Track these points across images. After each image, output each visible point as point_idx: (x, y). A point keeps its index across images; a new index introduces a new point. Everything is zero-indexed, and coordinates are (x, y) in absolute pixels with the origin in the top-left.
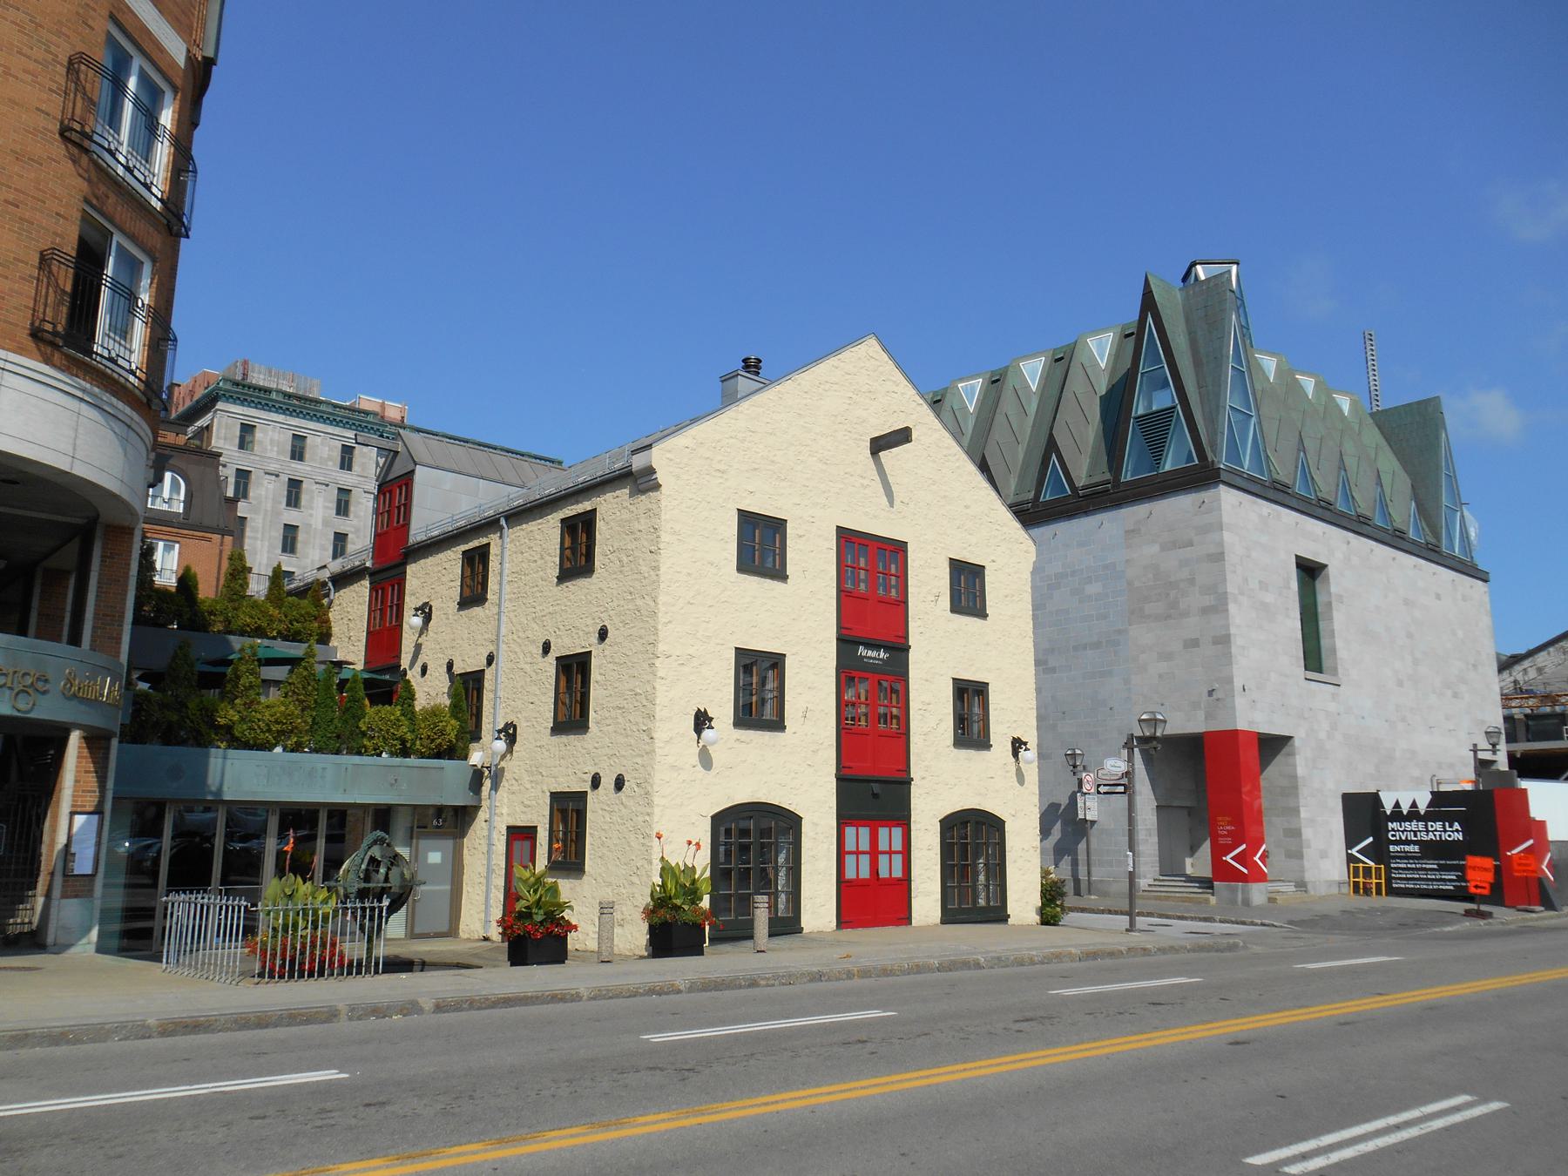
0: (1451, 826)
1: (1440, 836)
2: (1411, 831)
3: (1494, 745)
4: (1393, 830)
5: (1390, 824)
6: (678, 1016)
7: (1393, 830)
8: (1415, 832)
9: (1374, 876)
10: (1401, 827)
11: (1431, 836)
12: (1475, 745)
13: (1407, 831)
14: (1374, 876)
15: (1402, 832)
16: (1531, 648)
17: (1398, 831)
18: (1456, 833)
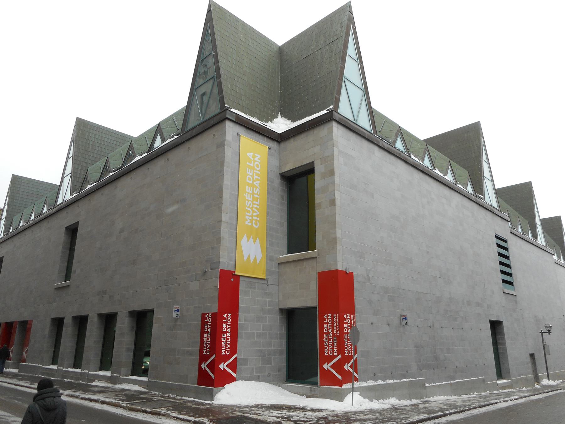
0: (224, 318)
1: (229, 325)
3: (549, 331)
5: (222, 354)
6: (301, 59)
9: (244, 304)
11: (229, 330)
12: (549, 334)
13: (226, 344)
14: (244, 304)
15: (329, 347)
17: (226, 348)
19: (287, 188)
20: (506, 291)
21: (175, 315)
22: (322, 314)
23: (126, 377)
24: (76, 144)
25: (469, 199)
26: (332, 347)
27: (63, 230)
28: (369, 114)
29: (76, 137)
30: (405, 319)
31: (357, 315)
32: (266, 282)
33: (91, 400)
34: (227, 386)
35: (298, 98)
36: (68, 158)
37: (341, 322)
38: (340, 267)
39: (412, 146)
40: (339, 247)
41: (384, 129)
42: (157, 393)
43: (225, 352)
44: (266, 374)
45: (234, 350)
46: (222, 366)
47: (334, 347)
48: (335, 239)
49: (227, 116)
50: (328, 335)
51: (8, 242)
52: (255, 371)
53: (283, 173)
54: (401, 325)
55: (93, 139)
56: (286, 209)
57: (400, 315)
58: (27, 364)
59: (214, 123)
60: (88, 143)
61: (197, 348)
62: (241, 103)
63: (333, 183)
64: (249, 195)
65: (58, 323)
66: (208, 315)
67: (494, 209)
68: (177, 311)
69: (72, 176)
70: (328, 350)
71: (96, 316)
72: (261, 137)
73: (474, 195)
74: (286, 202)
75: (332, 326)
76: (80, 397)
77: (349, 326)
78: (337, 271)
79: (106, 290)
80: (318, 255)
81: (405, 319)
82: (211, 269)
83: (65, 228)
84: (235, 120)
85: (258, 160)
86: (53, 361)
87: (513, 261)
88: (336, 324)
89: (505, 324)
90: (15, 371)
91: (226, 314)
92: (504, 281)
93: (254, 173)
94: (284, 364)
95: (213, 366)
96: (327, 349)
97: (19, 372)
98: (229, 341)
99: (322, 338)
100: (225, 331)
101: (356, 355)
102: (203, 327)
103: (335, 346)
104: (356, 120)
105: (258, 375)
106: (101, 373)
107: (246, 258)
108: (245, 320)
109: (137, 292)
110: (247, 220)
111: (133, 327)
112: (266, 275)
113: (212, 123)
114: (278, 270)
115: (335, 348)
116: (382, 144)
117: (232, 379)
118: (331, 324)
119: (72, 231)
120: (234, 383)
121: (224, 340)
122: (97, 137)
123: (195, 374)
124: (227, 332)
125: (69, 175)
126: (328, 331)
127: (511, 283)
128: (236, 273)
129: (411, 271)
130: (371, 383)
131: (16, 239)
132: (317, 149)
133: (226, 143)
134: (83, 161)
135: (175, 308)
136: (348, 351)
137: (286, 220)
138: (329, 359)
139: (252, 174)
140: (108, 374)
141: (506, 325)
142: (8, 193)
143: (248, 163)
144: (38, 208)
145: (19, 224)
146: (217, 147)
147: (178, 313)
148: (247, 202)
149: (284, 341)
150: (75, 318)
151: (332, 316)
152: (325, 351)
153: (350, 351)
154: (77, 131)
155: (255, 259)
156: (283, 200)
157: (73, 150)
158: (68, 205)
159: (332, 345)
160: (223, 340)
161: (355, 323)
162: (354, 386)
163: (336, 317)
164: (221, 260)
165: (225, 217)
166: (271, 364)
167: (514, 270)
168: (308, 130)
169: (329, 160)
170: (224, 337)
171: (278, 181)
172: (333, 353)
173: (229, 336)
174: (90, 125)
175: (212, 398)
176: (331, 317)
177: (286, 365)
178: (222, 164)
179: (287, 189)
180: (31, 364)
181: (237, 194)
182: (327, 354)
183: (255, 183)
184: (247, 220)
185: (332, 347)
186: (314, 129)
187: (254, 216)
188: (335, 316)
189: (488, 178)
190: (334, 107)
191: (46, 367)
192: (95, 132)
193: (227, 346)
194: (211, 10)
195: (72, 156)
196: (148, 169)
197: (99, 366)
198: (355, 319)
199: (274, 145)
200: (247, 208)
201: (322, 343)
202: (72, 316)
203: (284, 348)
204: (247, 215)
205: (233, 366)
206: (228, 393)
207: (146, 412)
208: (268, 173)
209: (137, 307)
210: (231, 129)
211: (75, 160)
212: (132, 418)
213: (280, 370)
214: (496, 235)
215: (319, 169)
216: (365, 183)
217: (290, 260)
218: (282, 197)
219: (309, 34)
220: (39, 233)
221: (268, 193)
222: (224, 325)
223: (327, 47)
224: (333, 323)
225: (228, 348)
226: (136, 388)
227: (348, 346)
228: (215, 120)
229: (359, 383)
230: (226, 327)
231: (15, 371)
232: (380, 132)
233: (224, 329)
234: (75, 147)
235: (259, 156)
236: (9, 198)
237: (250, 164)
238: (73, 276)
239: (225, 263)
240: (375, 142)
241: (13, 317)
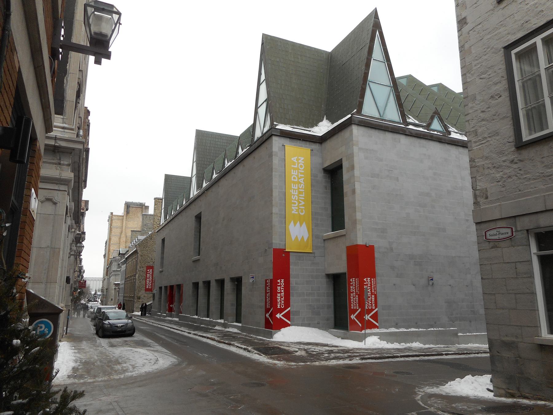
0: (365, 282)
1: (282, 287)
2: (281, 299)
4: (149, 287)
5: (278, 307)
7: (149, 287)
8: (150, 281)
10: (279, 303)
11: (282, 291)
13: (281, 300)
15: (281, 302)
16: (116, 7)
17: (281, 304)
18: (368, 280)
21: (251, 280)
22: (349, 279)
23: (231, 323)
24: (197, 151)
26: (370, 302)
27: (194, 218)
28: (398, 106)
30: (432, 280)
31: (378, 278)
32: (313, 255)
33: (203, 337)
34: (283, 330)
37: (361, 284)
38: (360, 242)
40: (359, 227)
42: (245, 334)
43: (280, 306)
44: (316, 322)
45: (287, 304)
46: (278, 316)
47: (373, 303)
48: (356, 220)
50: (281, 294)
52: (306, 320)
54: (429, 285)
56: (329, 196)
57: (428, 277)
58: (183, 315)
60: (206, 148)
61: (264, 304)
63: (354, 176)
64: (294, 190)
66: (268, 281)
68: (253, 278)
70: (281, 304)
75: (371, 287)
76: (199, 335)
77: (354, 287)
78: (357, 245)
80: (346, 233)
81: (432, 280)
82: (269, 248)
84: (279, 135)
85: (302, 162)
86: (221, 316)
88: (374, 286)
90: (177, 319)
91: (296, 157)
93: (298, 172)
94: (332, 316)
95: (272, 315)
96: (367, 304)
97: (179, 320)
98: (283, 298)
99: (350, 296)
100: (280, 291)
101: (377, 308)
102: (266, 289)
103: (373, 302)
104: (382, 115)
106: (219, 321)
107: (293, 238)
108: (296, 284)
110: (293, 210)
111: (234, 289)
112: (313, 250)
114: (323, 245)
115: (373, 304)
117: (287, 325)
118: (303, 171)
119: (198, 218)
120: (288, 327)
121: (279, 298)
122: (212, 142)
123: (263, 322)
124: (281, 292)
125: (262, 82)
126: (281, 291)
128: (286, 250)
130: (393, 330)
133: (273, 154)
135: (251, 276)
136: (354, 305)
138: (354, 311)
139: (296, 174)
140: (222, 321)
142: (164, 189)
143: (292, 166)
147: (254, 279)
148: (293, 196)
149: (331, 298)
151: (371, 280)
152: (293, 208)
153: (355, 306)
155: (303, 238)
159: (371, 301)
160: (293, 193)
161: (376, 284)
162: (366, 332)
163: (374, 280)
164: (274, 241)
165: (275, 210)
168: (338, 133)
169: (351, 157)
170: (278, 296)
171: (321, 175)
172: (372, 307)
173: (283, 295)
175: (272, 337)
176: (370, 280)
178: (271, 170)
180: (184, 315)
181: (284, 191)
182: (297, 213)
183: (300, 180)
184: (293, 210)
185: (370, 302)
187: (300, 206)
188: (372, 279)
190: (357, 110)
191: (192, 317)
193: (281, 302)
196: (234, 173)
197: (219, 316)
198: (376, 281)
199: (316, 147)
200: (292, 201)
201: (350, 299)
202: (230, 278)
203: (332, 303)
204: (294, 206)
205: (287, 316)
206: (283, 334)
207: (225, 343)
208: (311, 170)
210: (276, 142)
212: (218, 346)
213: (328, 320)
217: (331, 237)
218: (326, 188)
221: (312, 185)
222: (279, 288)
224: (371, 284)
225: (282, 304)
226: (235, 330)
227: (268, 301)
229: (379, 330)
230: (280, 289)
231: (177, 319)
233: (279, 290)
234: (197, 154)
235: (303, 158)
236: (165, 193)
237: (295, 166)
239: (277, 243)
241: (174, 282)
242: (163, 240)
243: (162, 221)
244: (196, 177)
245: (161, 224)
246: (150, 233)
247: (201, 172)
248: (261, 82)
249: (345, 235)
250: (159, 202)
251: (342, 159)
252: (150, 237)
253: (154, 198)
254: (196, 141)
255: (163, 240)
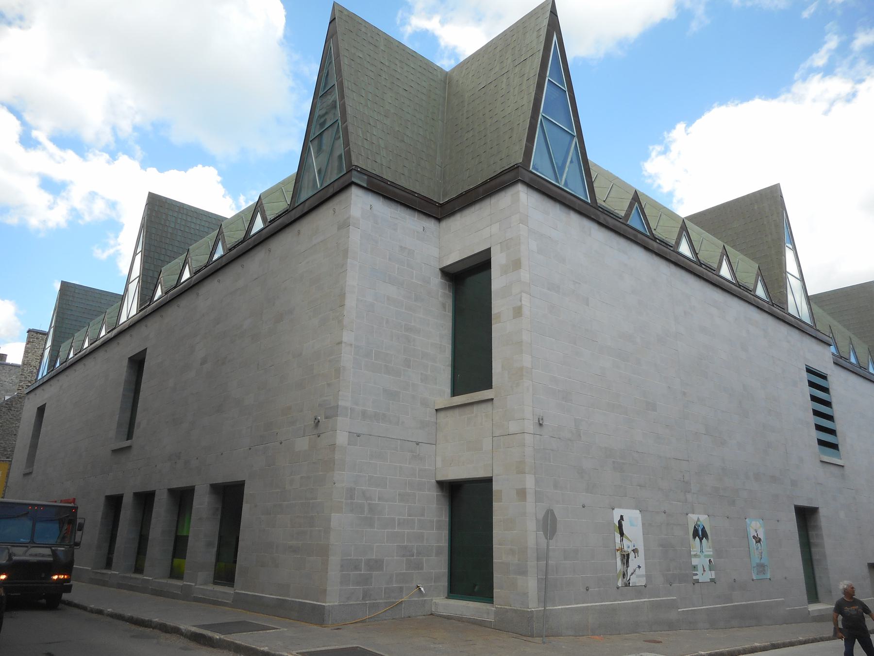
19: (452, 291)
20: (826, 459)
24: (147, 232)
25: (758, 307)
27: (125, 362)
29: (147, 222)
35: (471, 151)
36: (135, 254)
39: (661, 223)
41: (610, 196)
49: (354, 180)
51: (52, 382)
53: (444, 267)
55: (172, 225)
56: (449, 324)
59: (335, 191)
62: (378, 160)
65: (114, 503)
67: (803, 325)
69: (141, 281)
71: (166, 492)
72: (409, 211)
73: (768, 303)
74: (449, 314)
79: (180, 453)
82: (326, 418)
83: (128, 359)
84: (365, 186)
87: (837, 410)
89: (823, 512)
92: (821, 443)
105: (400, 586)
108: (379, 499)
109: (222, 454)
113: (331, 191)
116: (604, 219)
119: (137, 363)
125: (136, 279)
127: (834, 446)
129: (654, 422)
131: (63, 378)
132: (495, 228)
134: (157, 258)
137: (450, 342)
141: (824, 513)
144: (94, 329)
145: (69, 354)
146: (339, 228)
149: (445, 533)
150: (137, 495)
154: (149, 213)
156: (445, 311)
157: (143, 242)
158: (134, 324)
166: (422, 569)
167: (839, 425)
174: (169, 204)
177: (447, 571)
179: (452, 294)
186: (491, 197)
189: (795, 276)
192: (175, 214)
194: (335, 18)
195: (141, 251)
203: (445, 543)
209: (221, 478)
211: (145, 257)
214: (807, 367)
215: (498, 261)
216: (574, 281)
219: (491, 51)
220: (92, 366)
223: (517, 70)
228: (337, 186)
232: (604, 201)
238: (137, 432)
240: (592, 217)
242: (41, 410)
243: (44, 371)
244: (139, 282)
245: (39, 379)
246: (7, 398)
247: (151, 274)
248: (130, 281)
249: (492, 399)
250: (37, 338)
251: (490, 249)
252: (6, 404)
253: (27, 329)
254: (148, 214)
255: (41, 410)
